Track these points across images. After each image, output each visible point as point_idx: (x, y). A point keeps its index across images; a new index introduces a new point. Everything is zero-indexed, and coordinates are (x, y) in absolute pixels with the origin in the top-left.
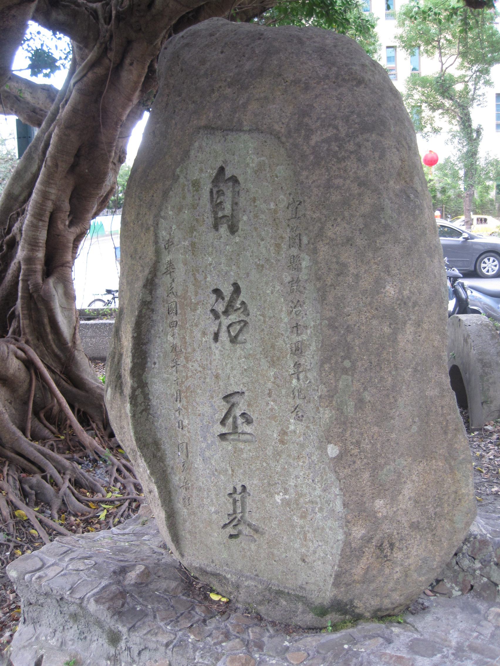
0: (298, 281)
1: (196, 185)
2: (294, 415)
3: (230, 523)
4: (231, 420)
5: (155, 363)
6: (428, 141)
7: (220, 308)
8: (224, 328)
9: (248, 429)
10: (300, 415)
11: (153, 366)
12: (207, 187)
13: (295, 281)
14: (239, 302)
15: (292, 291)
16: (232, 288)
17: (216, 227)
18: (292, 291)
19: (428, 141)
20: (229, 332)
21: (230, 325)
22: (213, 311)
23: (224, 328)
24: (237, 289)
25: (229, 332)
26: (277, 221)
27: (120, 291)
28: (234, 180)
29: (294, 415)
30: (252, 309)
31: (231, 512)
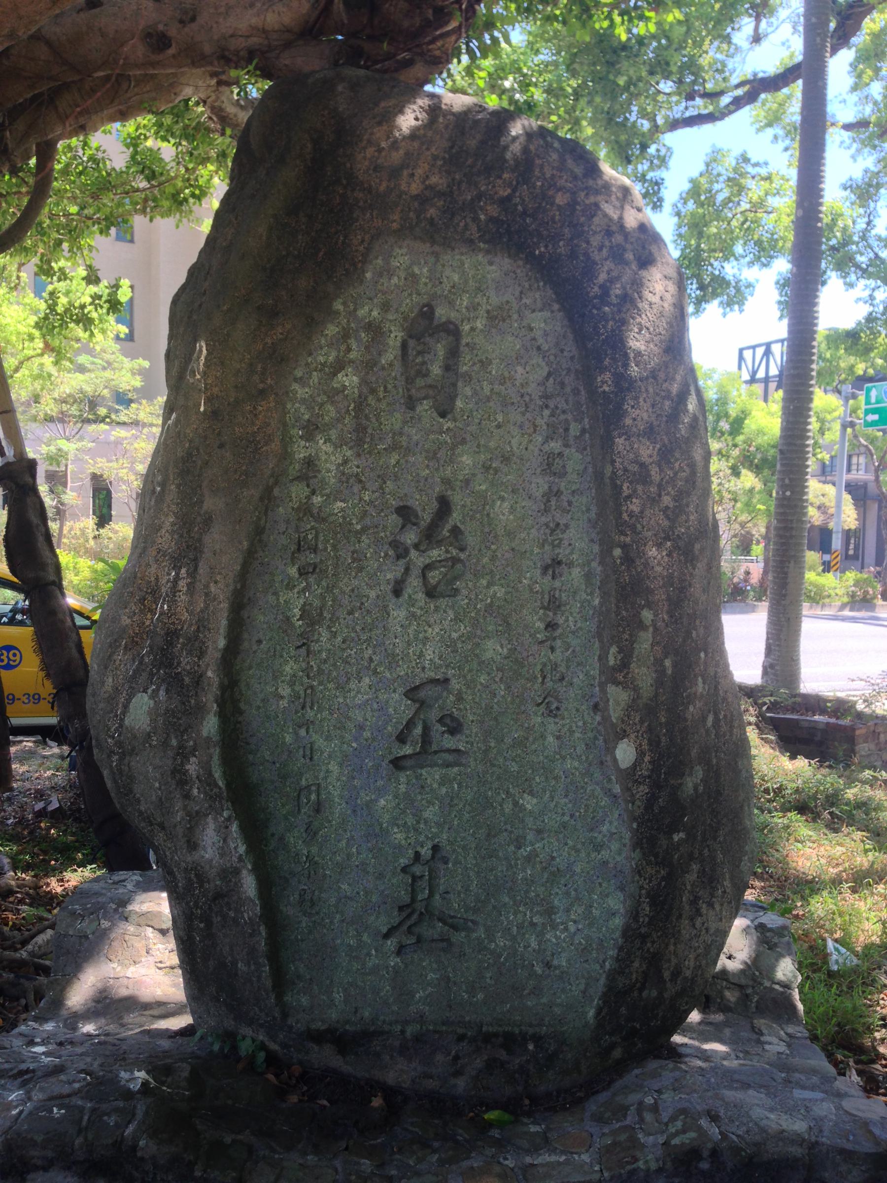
0: (558, 493)
1: (375, 330)
2: (542, 709)
3: (400, 924)
4: (418, 730)
5: (259, 642)
6: (724, 315)
7: (410, 537)
8: (415, 572)
9: (449, 742)
10: (553, 707)
11: (255, 647)
12: (395, 336)
13: (553, 493)
14: (448, 527)
15: (546, 510)
16: (435, 505)
17: (411, 403)
18: (546, 510)
19: (724, 315)
20: (424, 576)
21: (428, 567)
22: (395, 544)
23: (415, 572)
24: (444, 506)
25: (424, 576)
26: (527, 398)
27: (788, 339)
28: (452, 330)
29: (542, 709)
30: (471, 540)
31: (407, 899)
